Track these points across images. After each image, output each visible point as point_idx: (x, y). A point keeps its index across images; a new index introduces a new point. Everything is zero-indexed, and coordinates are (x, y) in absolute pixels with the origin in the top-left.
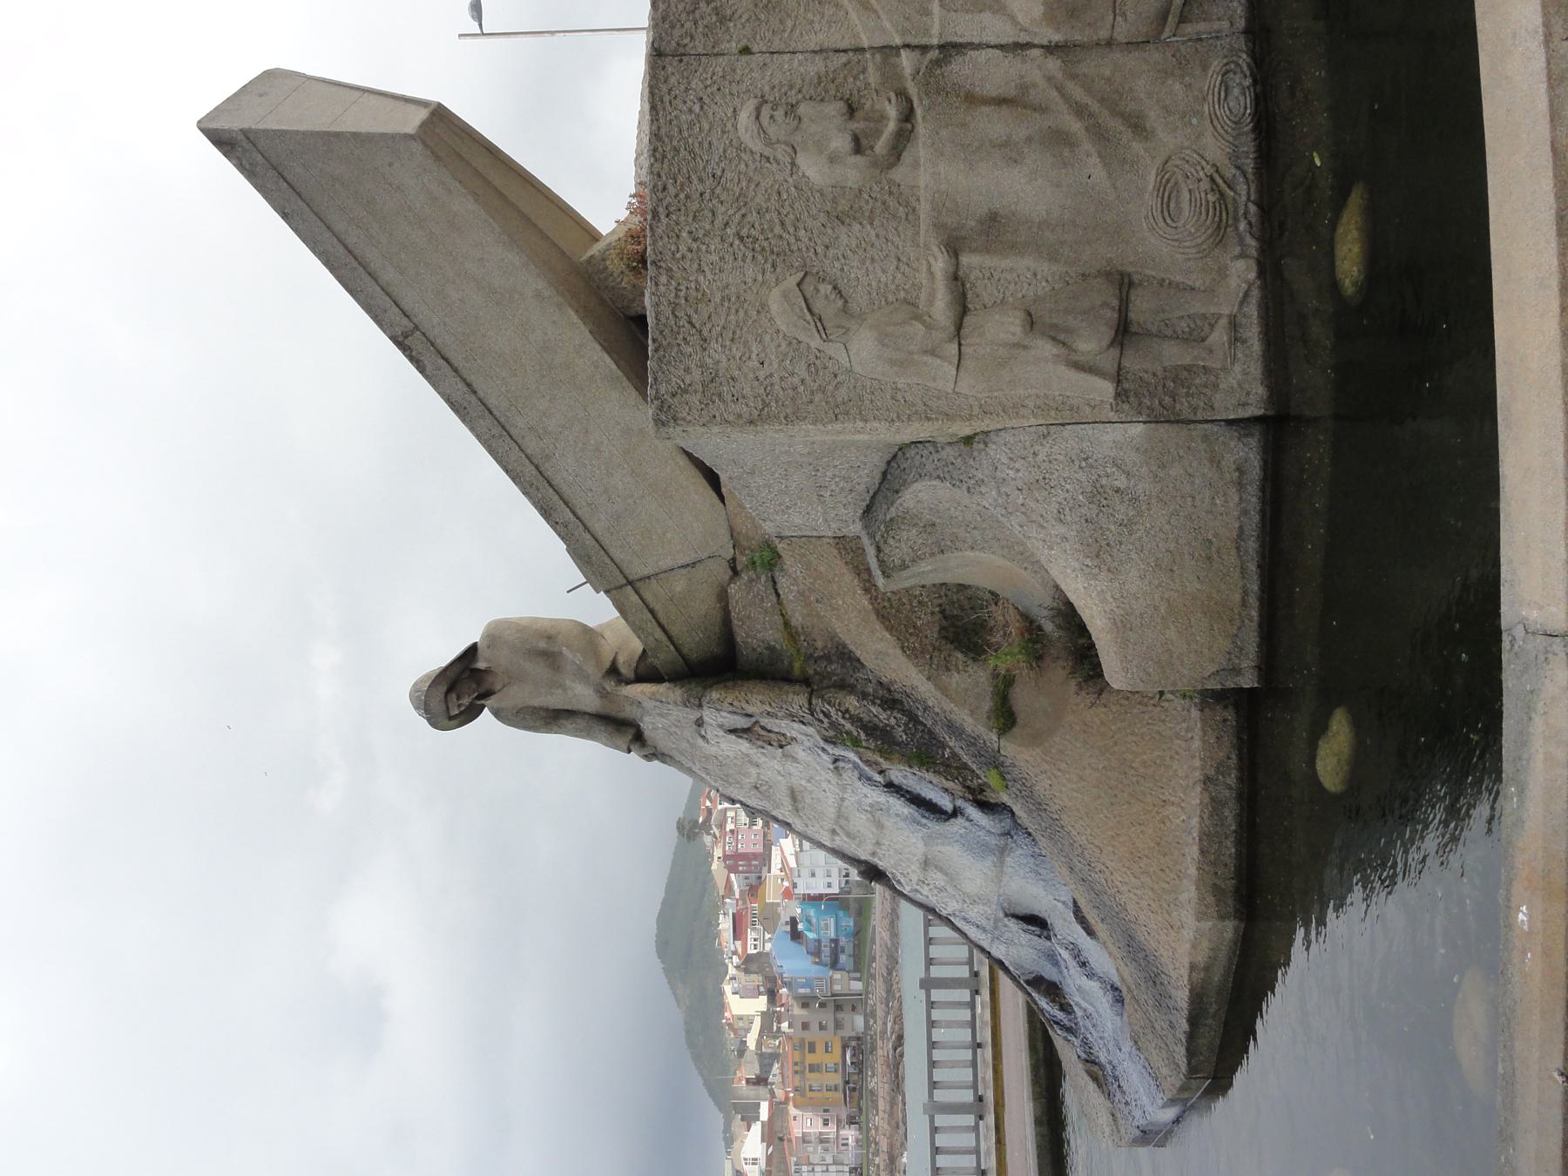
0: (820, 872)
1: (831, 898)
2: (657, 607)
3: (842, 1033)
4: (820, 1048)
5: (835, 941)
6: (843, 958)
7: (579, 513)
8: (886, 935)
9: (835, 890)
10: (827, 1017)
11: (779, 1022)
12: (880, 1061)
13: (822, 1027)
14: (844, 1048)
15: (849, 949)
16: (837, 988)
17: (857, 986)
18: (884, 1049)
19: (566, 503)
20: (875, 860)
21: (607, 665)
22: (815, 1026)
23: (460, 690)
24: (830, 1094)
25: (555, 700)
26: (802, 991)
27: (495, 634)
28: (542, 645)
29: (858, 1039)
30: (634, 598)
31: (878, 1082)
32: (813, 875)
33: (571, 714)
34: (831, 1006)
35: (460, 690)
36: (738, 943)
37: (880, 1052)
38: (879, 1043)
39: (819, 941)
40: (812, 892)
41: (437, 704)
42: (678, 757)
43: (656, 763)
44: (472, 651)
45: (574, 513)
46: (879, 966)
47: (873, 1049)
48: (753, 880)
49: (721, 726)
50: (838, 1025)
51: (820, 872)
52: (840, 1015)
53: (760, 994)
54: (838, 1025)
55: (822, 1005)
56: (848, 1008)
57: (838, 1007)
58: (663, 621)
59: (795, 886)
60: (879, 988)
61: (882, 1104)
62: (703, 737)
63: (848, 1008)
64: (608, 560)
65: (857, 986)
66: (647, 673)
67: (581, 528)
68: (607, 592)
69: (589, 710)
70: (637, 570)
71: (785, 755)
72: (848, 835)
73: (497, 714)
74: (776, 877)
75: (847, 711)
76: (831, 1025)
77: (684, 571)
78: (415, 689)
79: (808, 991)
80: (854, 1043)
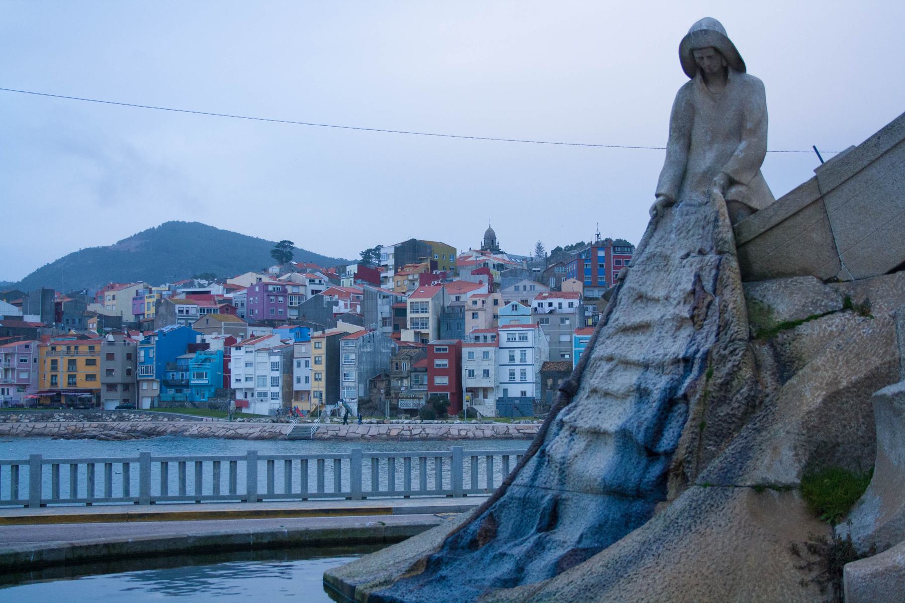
0: (250, 371)
1: (227, 381)
2: (798, 219)
3: (104, 390)
4: (91, 370)
5: (187, 385)
6: (172, 392)
7: (887, 156)
8: (194, 430)
9: (234, 385)
10: (119, 377)
11: (113, 333)
12: (80, 425)
13: (110, 372)
14: (90, 391)
15: (179, 397)
16: (144, 386)
17: (146, 404)
18: (89, 426)
19: (895, 146)
20: (583, 394)
21: (736, 178)
22: (110, 365)
23: (710, 59)
24: (48, 378)
25: (699, 134)
26: (142, 353)
27: (757, 88)
28: (749, 125)
29: (98, 404)
30: (808, 201)
31: (60, 422)
32: (247, 365)
33: (688, 147)
34: (129, 380)
35: (710, 59)
36: (183, 296)
37: (87, 424)
38: (95, 424)
39: (187, 370)
40: (232, 365)
41: (702, 42)
42: (657, 236)
43: (648, 218)
44: (740, 66)
45: (886, 152)
46: (165, 424)
47: (90, 419)
48: (240, 310)
49: (701, 269)
50: (111, 387)
51: (250, 371)
52: (120, 388)
53: (137, 316)
54: (111, 387)
55: (129, 372)
56: (127, 395)
57: (126, 387)
58: (786, 224)
59: (238, 348)
60: (145, 424)
61: (40, 425)
62: (687, 255)
63: (127, 395)
64: (843, 179)
65: (146, 404)
66: (739, 211)
67: (873, 158)
68: (816, 178)
69: (691, 163)
70: (832, 203)
71: (683, 319)
72: (611, 371)
73: (687, 86)
74: (245, 331)
75: (740, 369)
76: (110, 380)
77: (829, 240)
78: (716, 23)
79: (142, 359)
80: (94, 401)
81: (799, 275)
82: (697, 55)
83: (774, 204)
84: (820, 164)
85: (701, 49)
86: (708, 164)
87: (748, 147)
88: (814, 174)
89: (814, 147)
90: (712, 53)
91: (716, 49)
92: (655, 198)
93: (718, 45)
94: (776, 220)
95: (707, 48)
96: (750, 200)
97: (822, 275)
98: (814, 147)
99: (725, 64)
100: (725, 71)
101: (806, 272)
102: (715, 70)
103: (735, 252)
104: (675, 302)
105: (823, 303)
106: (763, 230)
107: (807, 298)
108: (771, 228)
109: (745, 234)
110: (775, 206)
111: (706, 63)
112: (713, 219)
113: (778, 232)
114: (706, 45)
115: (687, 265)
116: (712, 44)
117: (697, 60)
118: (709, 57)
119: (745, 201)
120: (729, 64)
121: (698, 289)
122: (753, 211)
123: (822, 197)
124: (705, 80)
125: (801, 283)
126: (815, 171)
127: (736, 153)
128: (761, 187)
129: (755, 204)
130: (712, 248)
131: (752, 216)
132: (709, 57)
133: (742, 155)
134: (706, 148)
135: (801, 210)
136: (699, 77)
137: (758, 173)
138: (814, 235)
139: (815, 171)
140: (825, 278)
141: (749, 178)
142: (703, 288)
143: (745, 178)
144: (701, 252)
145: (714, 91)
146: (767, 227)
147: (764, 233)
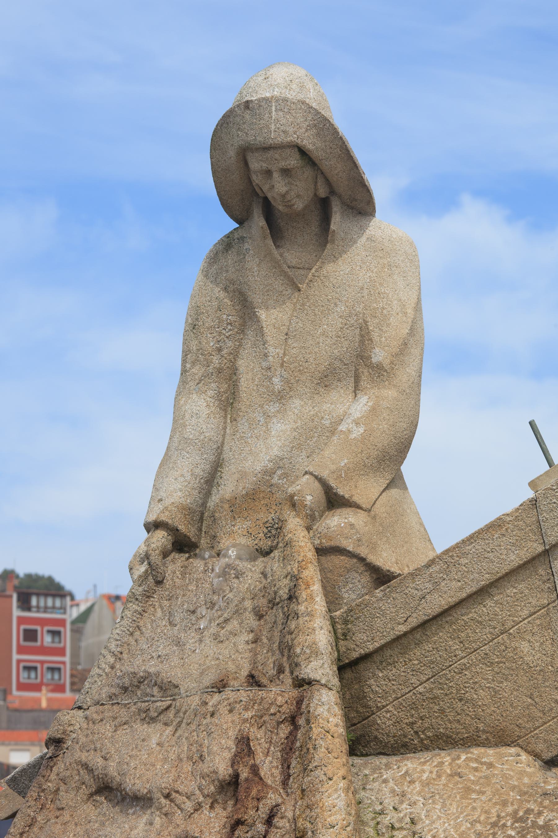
2: (490, 604)
21: (342, 491)
30: (514, 559)
35: (95, 586)
68: (534, 503)
81: (486, 744)
82: (256, 164)
83: (432, 563)
84: (546, 467)
85: (267, 149)
86: (275, 451)
87: (373, 410)
88: (531, 494)
89: (532, 424)
90: (293, 161)
91: (303, 152)
92: (144, 534)
93: (309, 142)
94: (437, 603)
95: (281, 147)
96: (373, 547)
97: (540, 747)
98: (532, 424)
99: (322, 192)
100: (323, 207)
101: (501, 738)
102: (299, 205)
103: (335, 681)
104: (189, 806)
105: (541, 822)
106: (403, 628)
107: (504, 803)
108: (424, 625)
109: (360, 637)
110: (434, 569)
111: (278, 187)
112: (283, 593)
113: (441, 636)
114: (281, 139)
115: (223, 710)
116: (292, 138)
117: (257, 179)
118: (286, 172)
119: (363, 551)
120: (332, 192)
121: (244, 774)
122: (381, 578)
123: (546, 553)
124: (275, 227)
125: (490, 765)
126: (533, 485)
127: (343, 427)
128: (398, 522)
129: (385, 560)
130: (281, 670)
131: (378, 593)
132: (286, 172)
133: (358, 432)
134: (273, 408)
135: (494, 584)
136: (258, 222)
137: (396, 481)
138: (525, 646)
139: (533, 485)
140: (548, 755)
141: (375, 491)
142: (255, 770)
143: (365, 490)
144: (253, 681)
145: (294, 262)
146: (414, 622)
147: (405, 634)
